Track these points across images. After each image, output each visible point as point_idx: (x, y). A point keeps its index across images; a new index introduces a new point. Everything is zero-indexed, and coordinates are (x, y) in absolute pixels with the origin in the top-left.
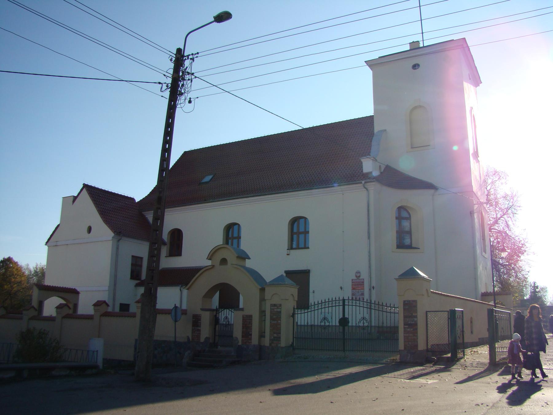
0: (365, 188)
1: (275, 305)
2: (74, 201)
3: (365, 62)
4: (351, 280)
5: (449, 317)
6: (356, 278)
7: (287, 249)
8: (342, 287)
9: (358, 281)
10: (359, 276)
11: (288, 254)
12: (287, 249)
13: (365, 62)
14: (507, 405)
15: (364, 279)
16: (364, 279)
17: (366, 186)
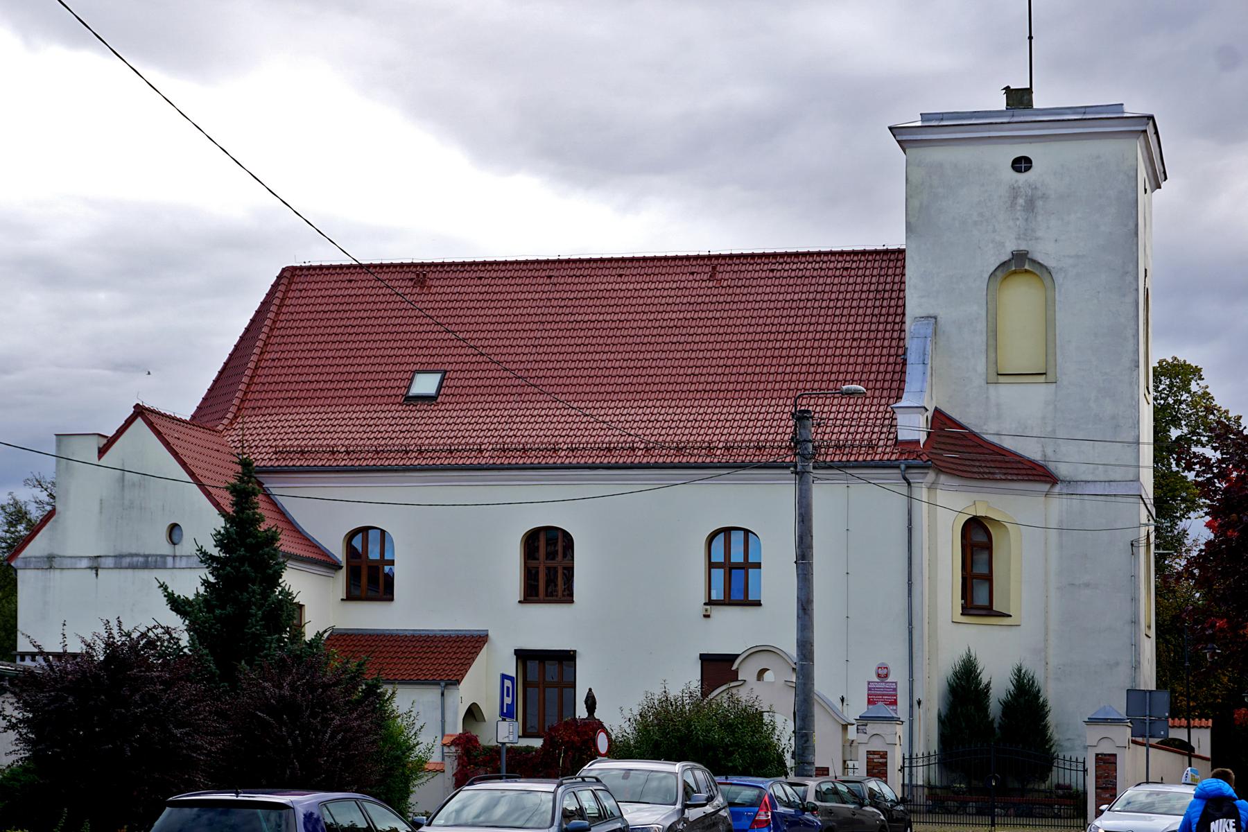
0: (905, 479)
1: (874, 753)
2: (102, 452)
3: (891, 128)
4: (866, 684)
5: (505, 711)
6: (878, 680)
7: (705, 604)
8: (845, 697)
9: (883, 685)
10: (886, 676)
11: (707, 616)
12: (705, 604)
13: (891, 128)
14: (973, 512)
15: (896, 683)
16: (896, 683)
17: (907, 476)
